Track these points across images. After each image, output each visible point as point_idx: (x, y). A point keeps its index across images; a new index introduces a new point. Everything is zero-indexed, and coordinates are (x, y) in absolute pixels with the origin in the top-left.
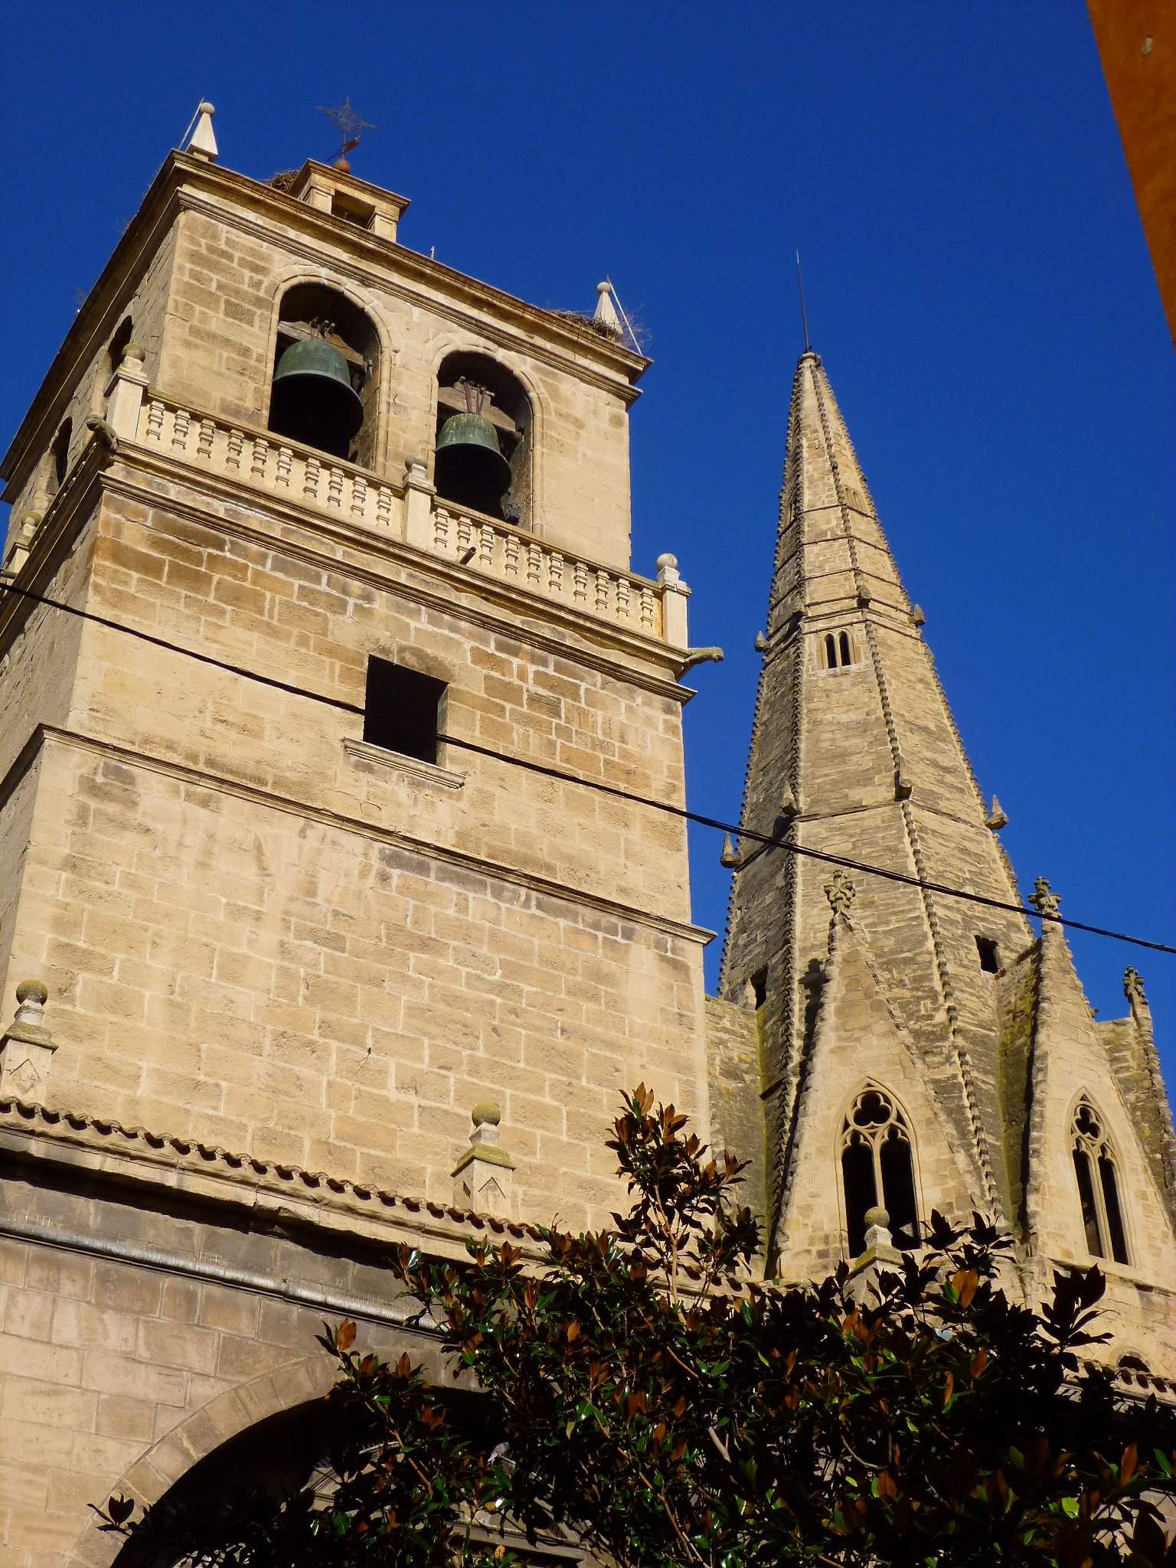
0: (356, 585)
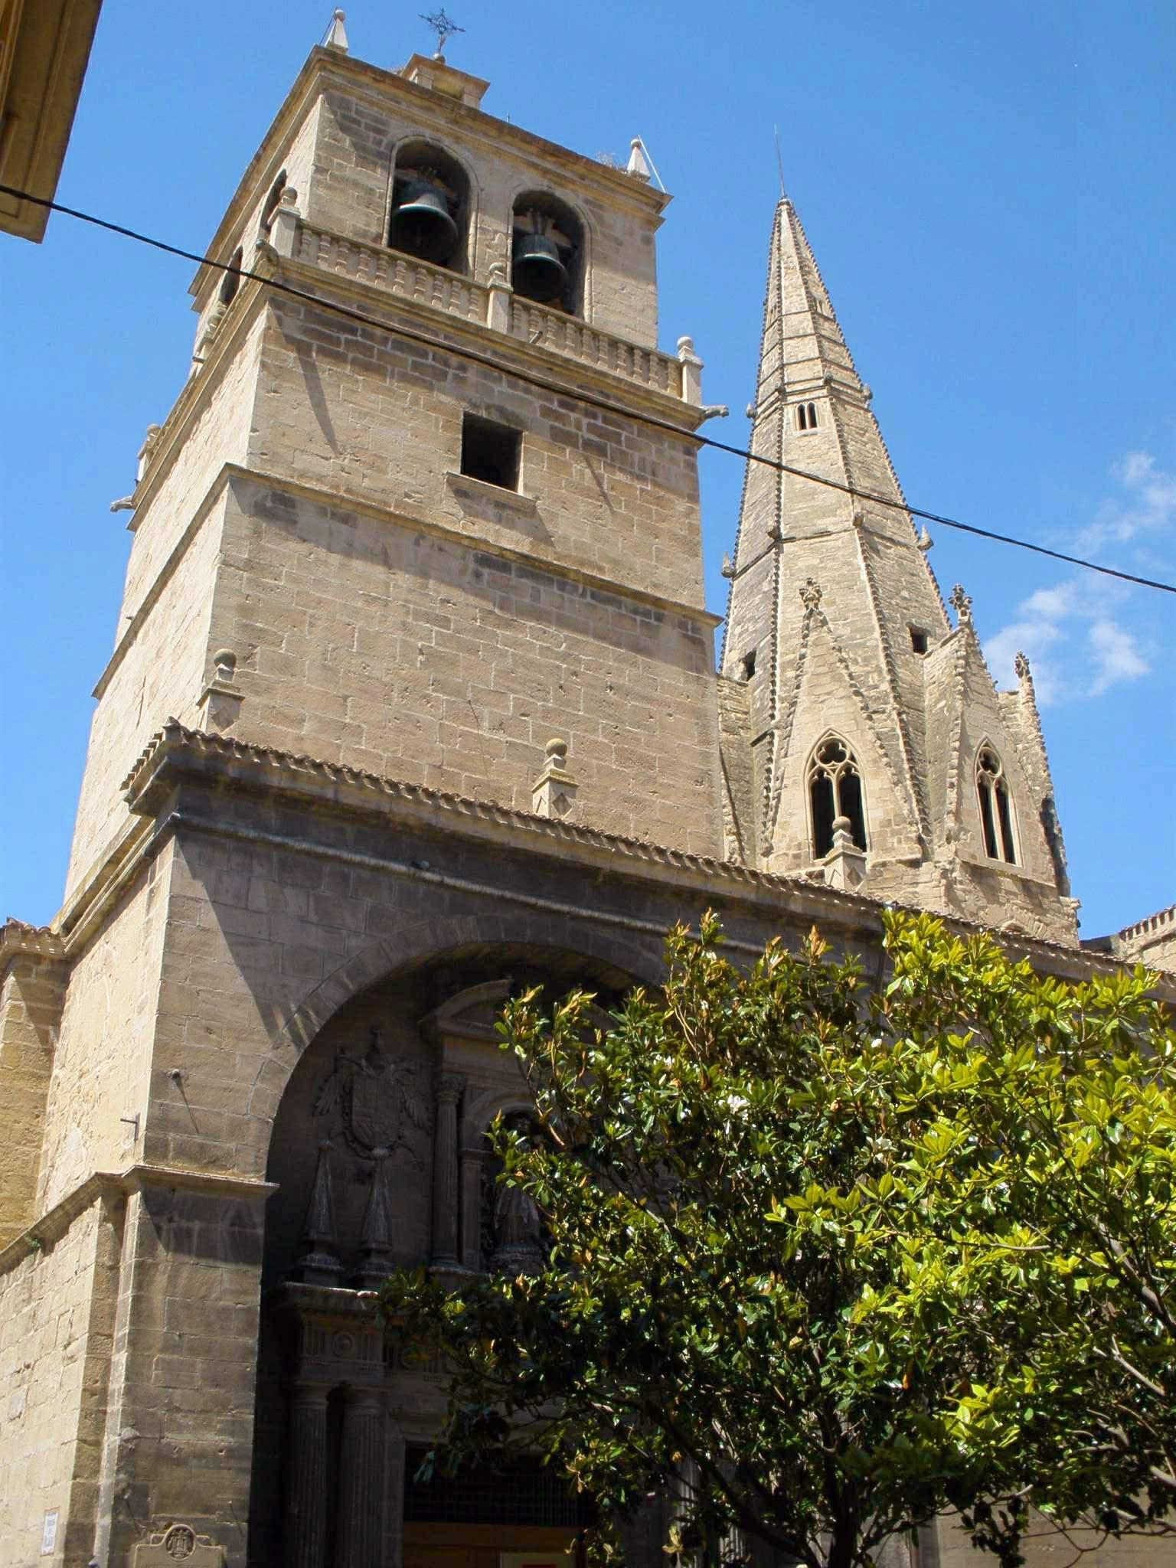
0: (455, 360)
